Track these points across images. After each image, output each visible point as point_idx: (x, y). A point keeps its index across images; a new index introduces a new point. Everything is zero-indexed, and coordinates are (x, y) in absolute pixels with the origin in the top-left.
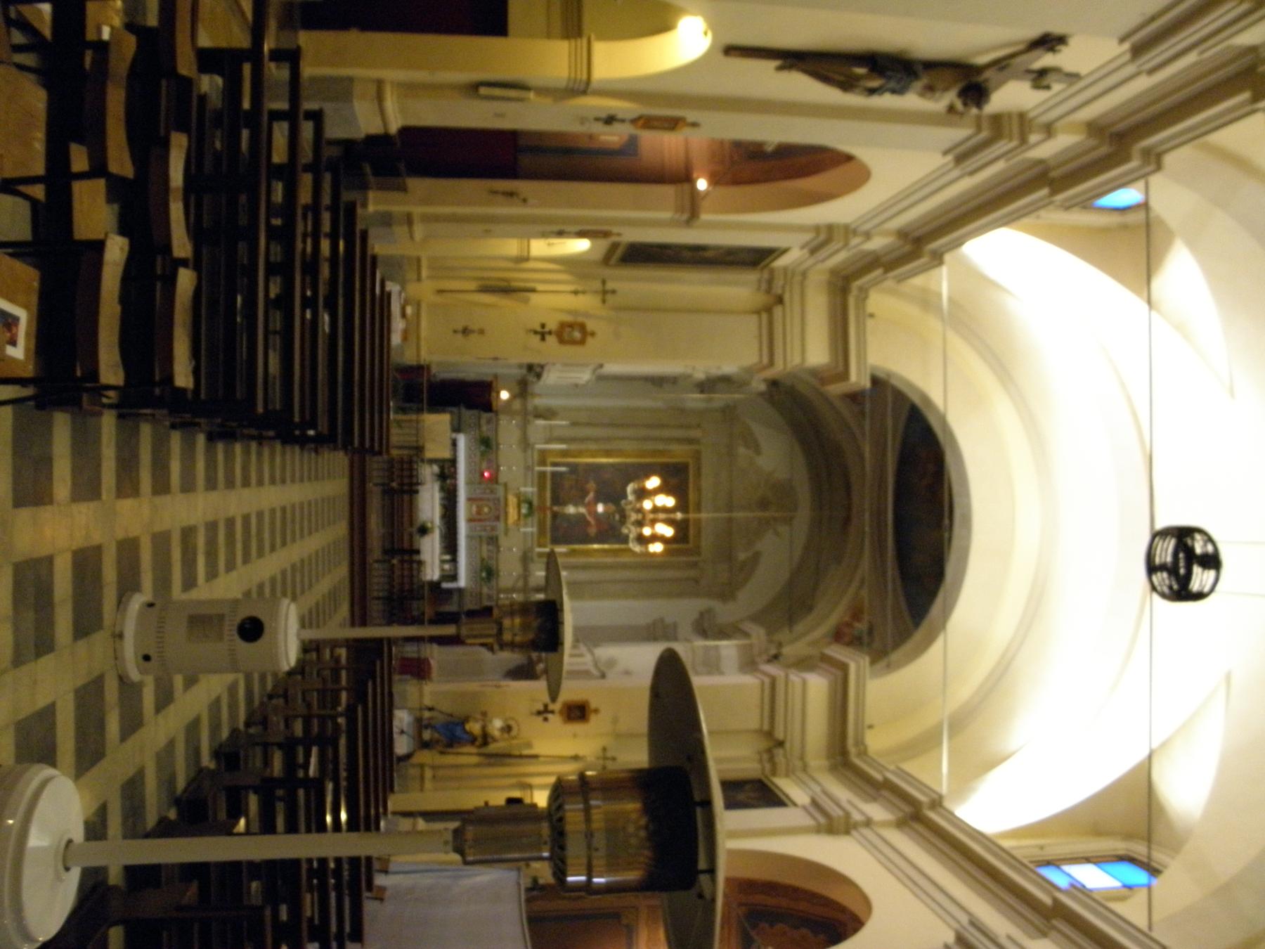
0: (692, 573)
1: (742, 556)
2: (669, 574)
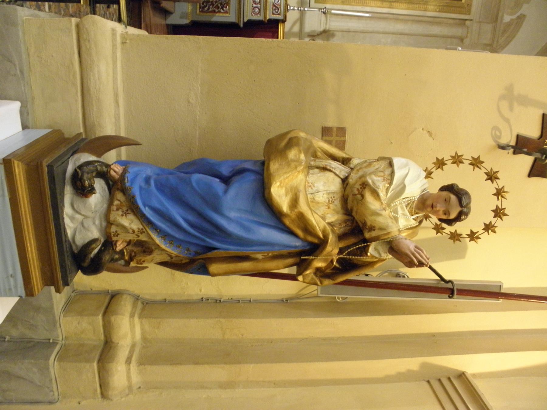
0: (459, 31)
1: (507, 18)
2: (436, 30)
